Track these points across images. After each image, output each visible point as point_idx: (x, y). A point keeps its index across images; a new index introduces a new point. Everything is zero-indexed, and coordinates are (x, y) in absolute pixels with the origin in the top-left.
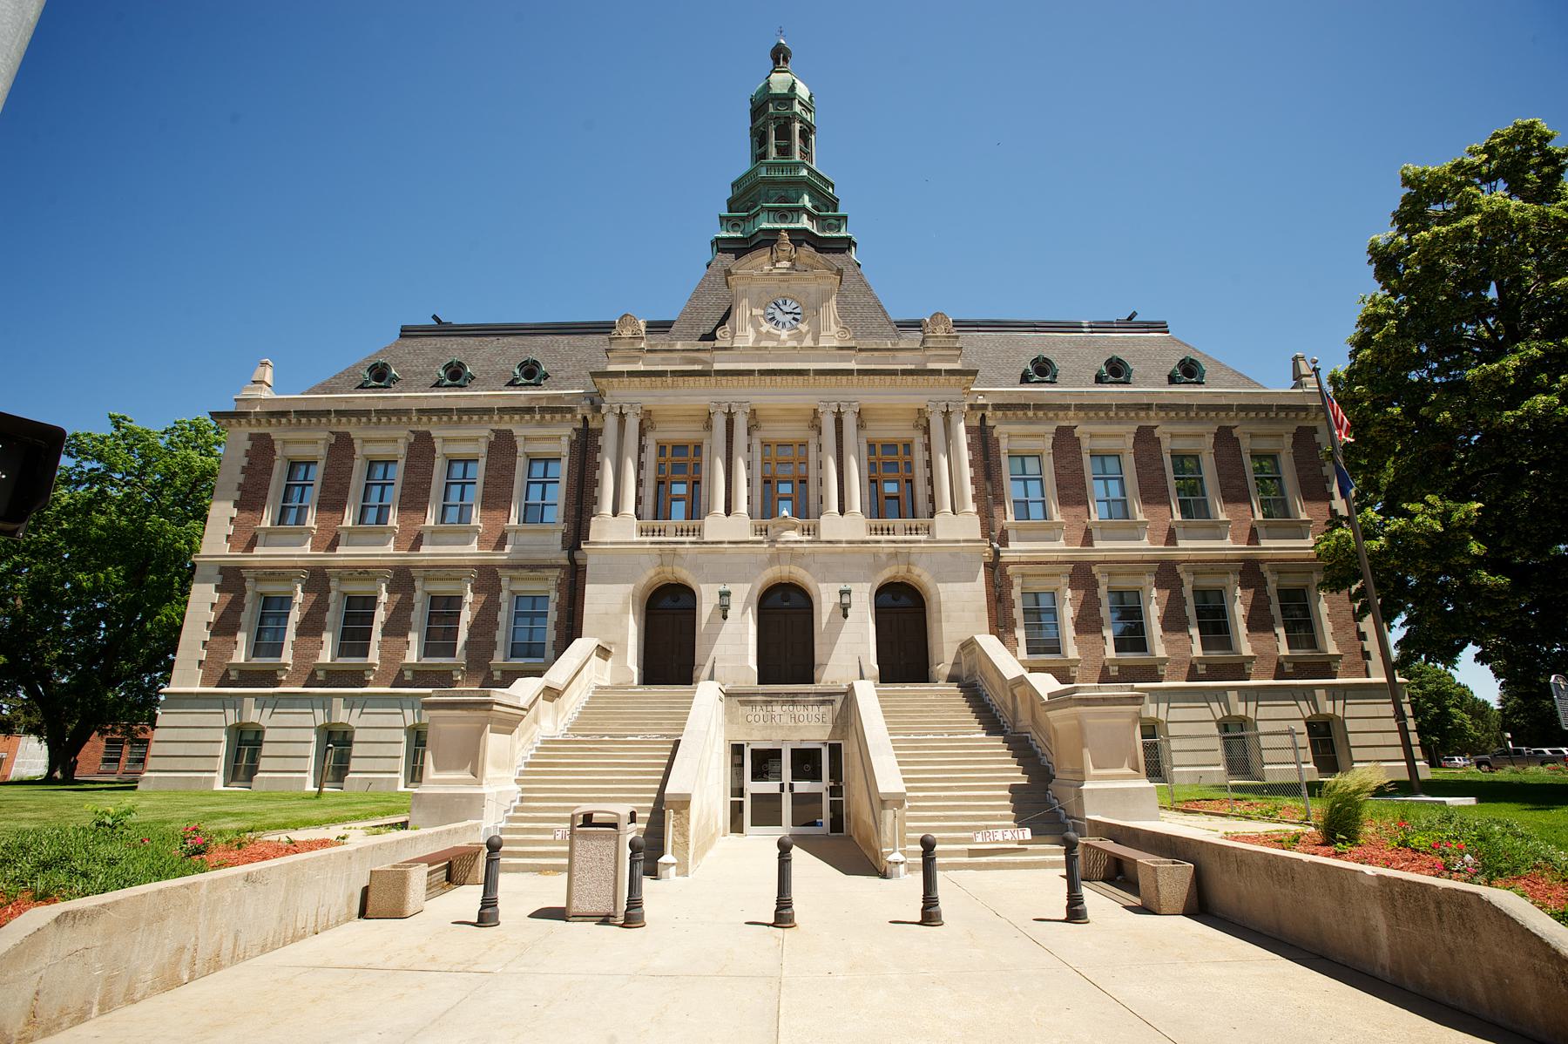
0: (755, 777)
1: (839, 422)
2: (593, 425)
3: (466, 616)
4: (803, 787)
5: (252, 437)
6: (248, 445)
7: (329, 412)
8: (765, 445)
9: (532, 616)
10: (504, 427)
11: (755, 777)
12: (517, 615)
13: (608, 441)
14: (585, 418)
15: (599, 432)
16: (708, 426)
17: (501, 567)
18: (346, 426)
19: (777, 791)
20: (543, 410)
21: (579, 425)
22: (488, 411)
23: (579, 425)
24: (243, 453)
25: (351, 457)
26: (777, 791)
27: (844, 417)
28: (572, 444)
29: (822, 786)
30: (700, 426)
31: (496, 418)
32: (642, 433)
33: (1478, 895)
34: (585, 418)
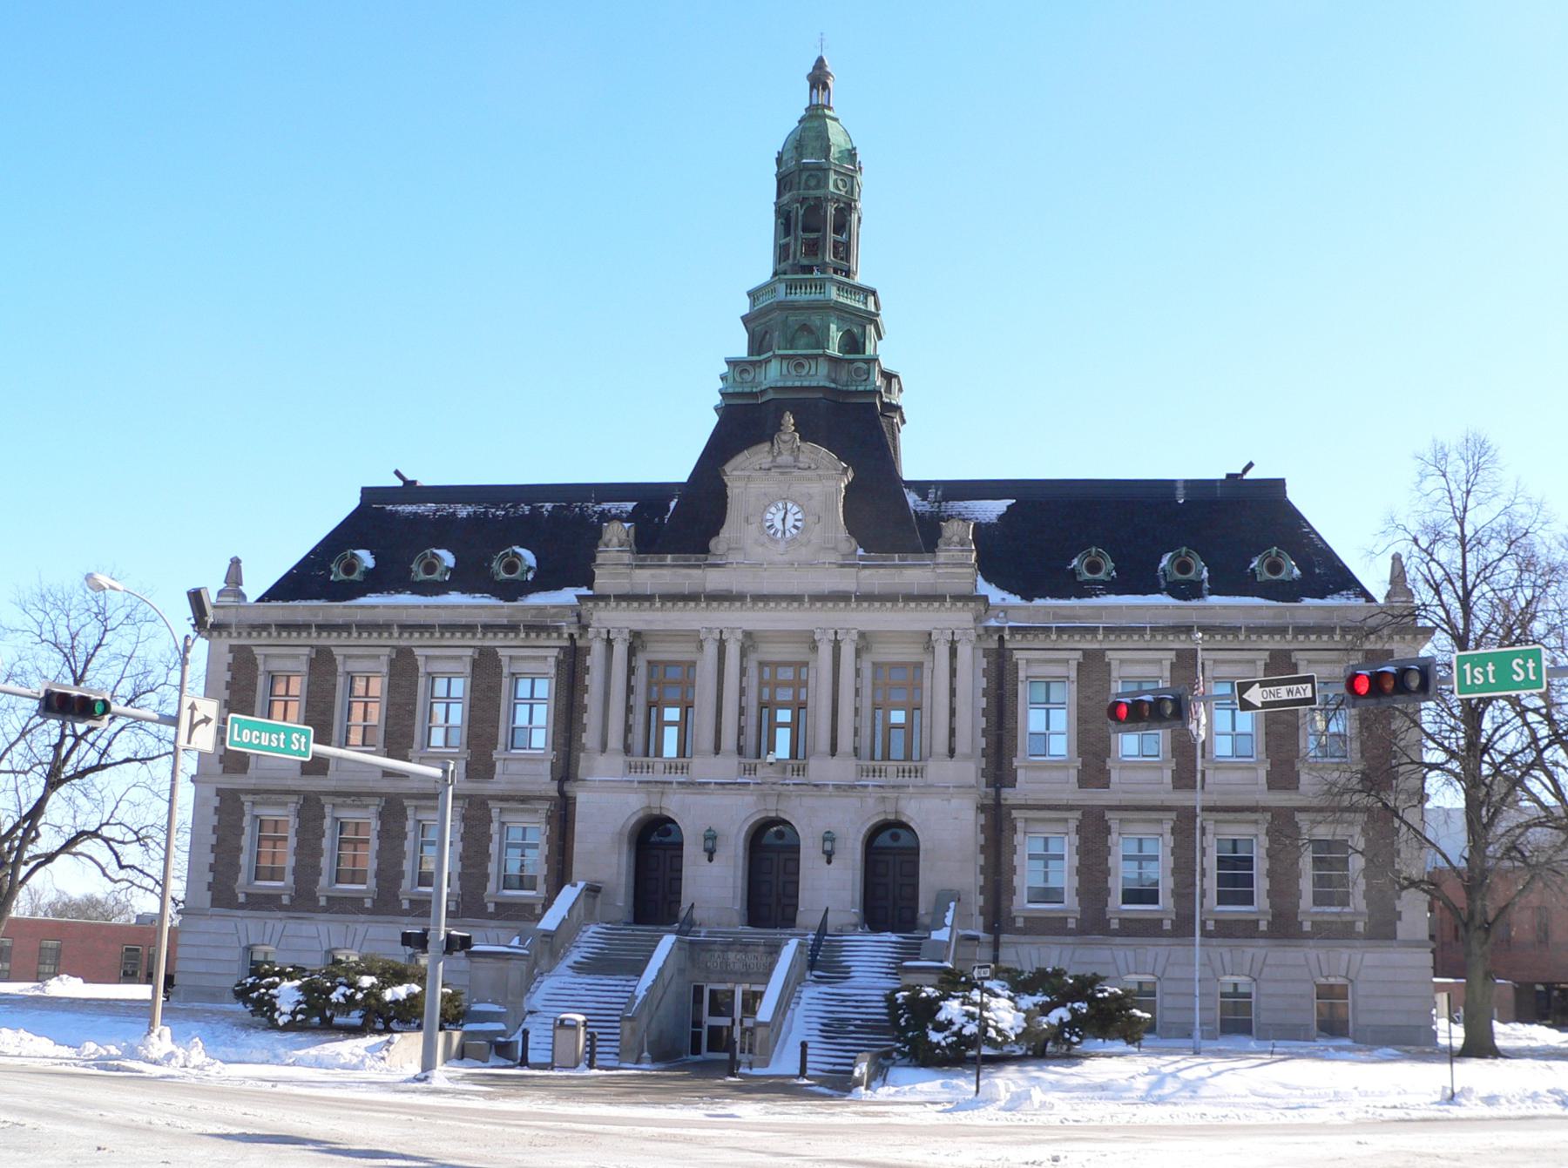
0: (711, 1014)
1: (722, 645)
2: (580, 643)
3: (1306, 886)
4: (724, 1021)
5: (232, 649)
6: (229, 658)
7: (433, 626)
8: (876, 666)
9: (275, 840)
10: (487, 643)
11: (711, 1014)
12: (341, 841)
13: (595, 660)
14: (571, 636)
15: (588, 650)
16: (814, 647)
17: (327, 794)
18: (325, 640)
19: (149, 997)
20: (529, 628)
21: (566, 643)
22: (469, 628)
23: (566, 643)
24: (225, 667)
25: (334, 673)
26: (149, 997)
27: (960, 647)
28: (559, 664)
29: (709, 1021)
30: (919, 648)
31: (1054, 637)
32: (632, 652)
33: (88, 979)
34: (571, 636)
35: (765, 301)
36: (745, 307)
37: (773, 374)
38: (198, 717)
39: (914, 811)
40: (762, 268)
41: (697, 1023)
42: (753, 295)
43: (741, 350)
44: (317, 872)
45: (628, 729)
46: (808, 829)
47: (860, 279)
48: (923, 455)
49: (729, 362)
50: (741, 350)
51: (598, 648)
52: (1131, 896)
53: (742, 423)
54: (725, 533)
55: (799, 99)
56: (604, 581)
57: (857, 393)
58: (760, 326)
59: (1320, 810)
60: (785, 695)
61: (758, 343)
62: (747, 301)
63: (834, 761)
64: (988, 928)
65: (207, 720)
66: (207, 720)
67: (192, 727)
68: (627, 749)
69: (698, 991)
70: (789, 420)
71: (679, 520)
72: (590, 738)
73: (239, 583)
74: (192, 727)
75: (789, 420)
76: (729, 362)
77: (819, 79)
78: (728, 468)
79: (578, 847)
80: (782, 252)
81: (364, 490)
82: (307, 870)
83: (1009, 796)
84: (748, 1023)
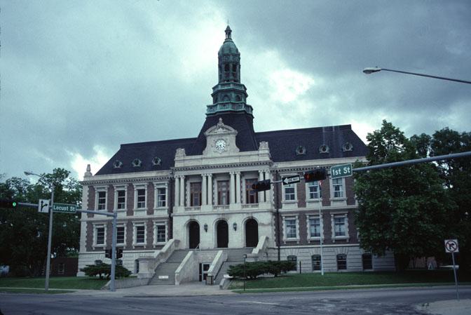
29: (204, 272)
35: (216, 90)
36: (212, 92)
37: (219, 109)
38: (44, 204)
39: (257, 217)
40: (216, 82)
41: (201, 272)
42: (214, 88)
43: (211, 103)
44: (92, 241)
45: (213, 199)
46: (202, 222)
47: (242, 83)
48: (260, 126)
49: (208, 106)
50: (211, 103)
51: (177, 180)
52: (337, 234)
53: (211, 120)
54: (206, 149)
55: (223, 37)
56: (177, 165)
57: (239, 111)
58: (216, 94)
59: (227, 214)
60: (224, 189)
61: (215, 101)
62: (212, 90)
63: (236, 204)
64: (277, 245)
65: (46, 205)
66: (46, 205)
67: (42, 207)
68: (213, 203)
69: (200, 265)
70: (221, 119)
71: (196, 146)
72: (176, 203)
73: (90, 170)
74: (42, 207)
75: (221, 119)
76: (208, 106)
77: (228, 32)
78: (256, 131)
79: (174, 230)
80: (220, 77)
81: (122, 146)
82: (303, 234)
83: (172, 214)
84: (205, 272)
